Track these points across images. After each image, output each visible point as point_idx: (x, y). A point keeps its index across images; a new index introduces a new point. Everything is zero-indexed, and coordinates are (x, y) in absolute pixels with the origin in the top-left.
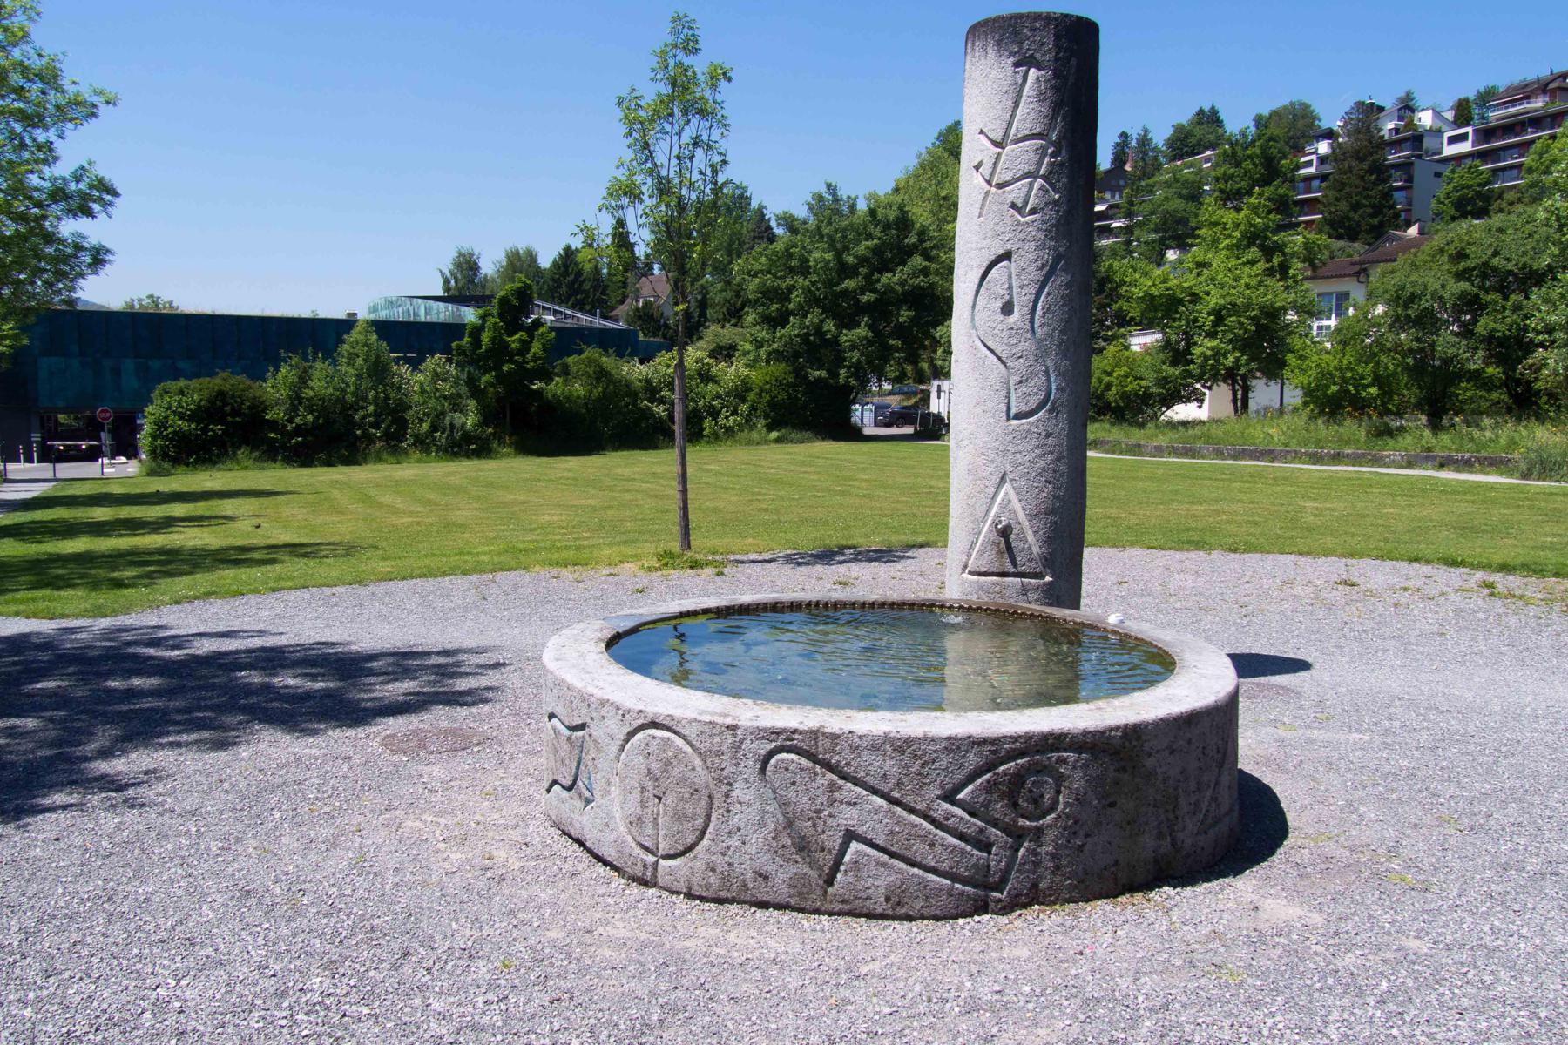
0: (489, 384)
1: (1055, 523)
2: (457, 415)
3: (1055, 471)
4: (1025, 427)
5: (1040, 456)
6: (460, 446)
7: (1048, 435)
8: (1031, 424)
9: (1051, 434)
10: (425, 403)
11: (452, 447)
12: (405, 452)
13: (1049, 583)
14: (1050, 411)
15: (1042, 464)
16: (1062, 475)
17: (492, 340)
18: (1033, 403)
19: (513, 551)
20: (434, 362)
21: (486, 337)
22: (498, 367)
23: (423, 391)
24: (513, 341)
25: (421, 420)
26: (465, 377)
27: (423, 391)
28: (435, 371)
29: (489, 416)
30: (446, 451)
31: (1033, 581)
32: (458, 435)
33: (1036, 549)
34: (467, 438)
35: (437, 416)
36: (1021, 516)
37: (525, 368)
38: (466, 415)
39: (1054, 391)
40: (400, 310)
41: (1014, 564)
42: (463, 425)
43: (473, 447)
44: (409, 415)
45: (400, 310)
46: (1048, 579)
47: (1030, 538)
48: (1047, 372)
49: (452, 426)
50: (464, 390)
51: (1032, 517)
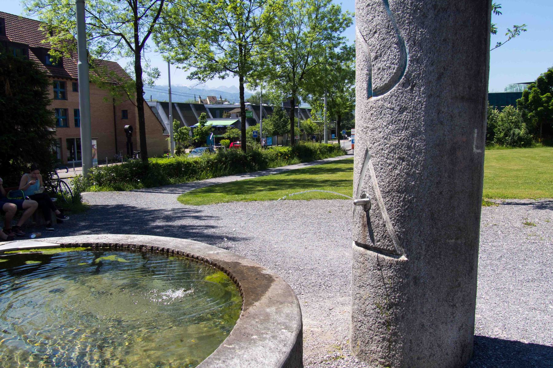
0: (532, 116)
1: (410, 202)
2: (517, 130)
3: (409, 148)
4: (380, 103)
5: (393, 132)
6: (517, 142)
7: (402, 111)
8: (384, 100)
9: (405, 109)
10: (503, 125)
11: (514, 143)
12: (493, 145)
13: (403, 263)
14: (404, 85)
15: (395, 140)
16: (419, 152)
17: (534, 97)
18: (386, 78)
19: (224, 186)
20: (508, 108)
21: (531, 97)
22: (536, 109)
23: (502, 120)
24: (544, 97)
25: (501, 132)
26: (521, 114)
27: (502, 120)
28: (509, 112)
29: (531, 130)
30: (510, 144)
31: (387, 258)
32: (516, 138)
33: (390, 227)
34: (520, 139)
35: (508, 130)
36: (378, 193)
37: (549, 109)
38: (521, 130)
39: (408, 63)
40: (515, 89)
41: (373, 241)
42: (519, 134)
43: (522, 143)
44: (495, 130)
45: (515, 89)
46: (404, 258)
47: (385, 215)
48: (400, 44)
49: (514, 134)
50: (521, 119)
51: (386, 193)
